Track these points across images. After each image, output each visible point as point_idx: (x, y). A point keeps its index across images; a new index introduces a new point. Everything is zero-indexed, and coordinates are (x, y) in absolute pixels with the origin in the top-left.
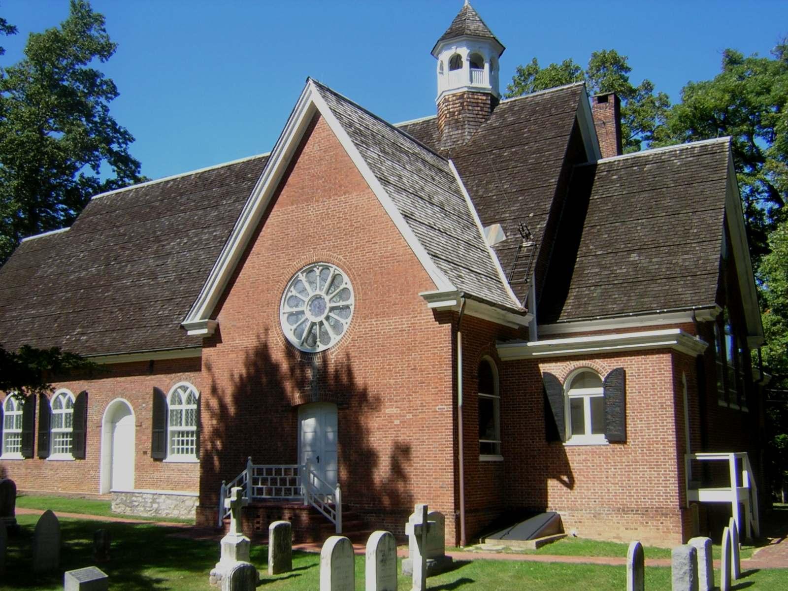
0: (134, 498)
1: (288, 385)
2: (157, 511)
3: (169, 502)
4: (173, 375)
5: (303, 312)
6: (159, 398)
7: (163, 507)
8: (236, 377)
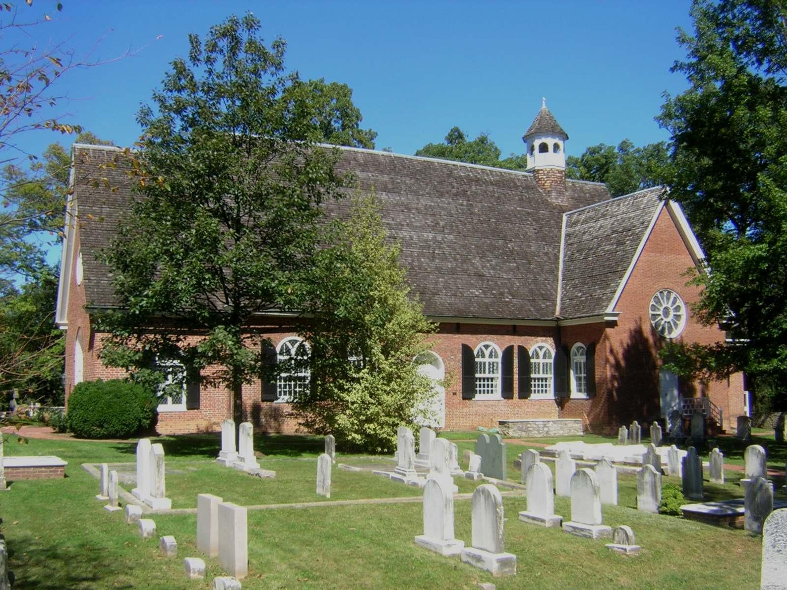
0: (529, 425)
1: (653, 351)
2: (547, 432)
3: (555, 425)
4: (479, 336)
5: (659, 315)
6: (467, 351)
7: (551, 429)
8: (625, 345)
